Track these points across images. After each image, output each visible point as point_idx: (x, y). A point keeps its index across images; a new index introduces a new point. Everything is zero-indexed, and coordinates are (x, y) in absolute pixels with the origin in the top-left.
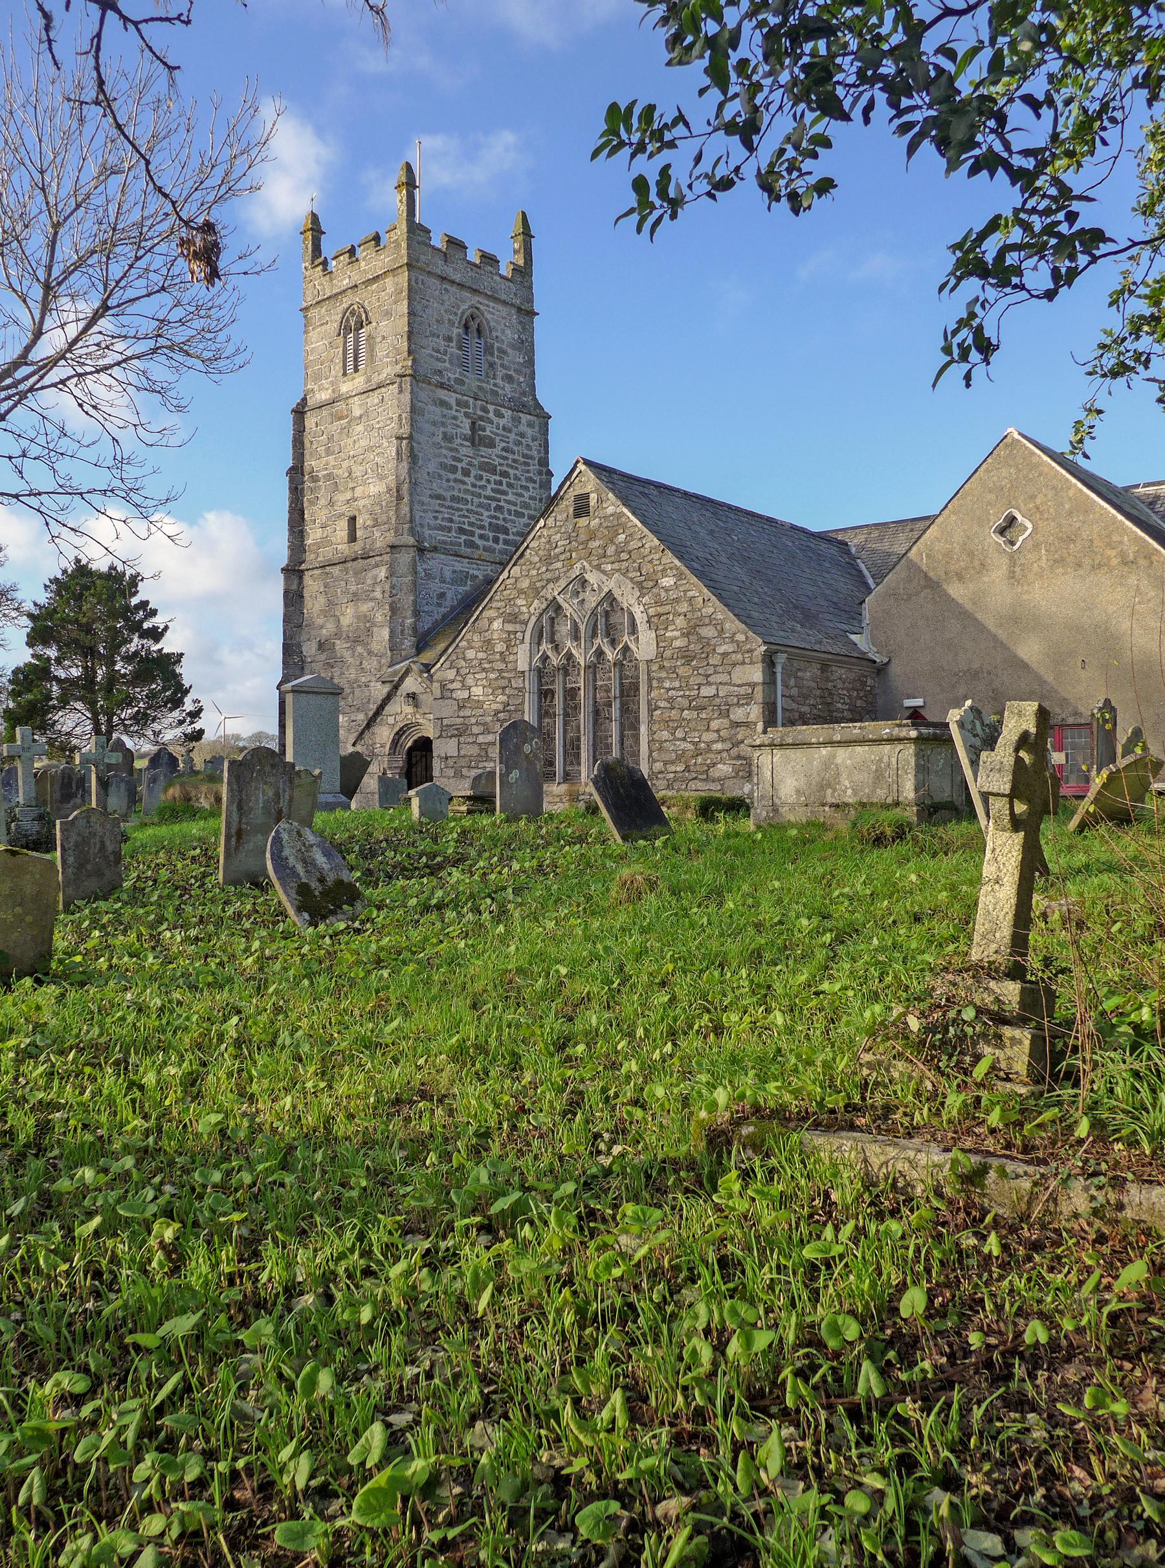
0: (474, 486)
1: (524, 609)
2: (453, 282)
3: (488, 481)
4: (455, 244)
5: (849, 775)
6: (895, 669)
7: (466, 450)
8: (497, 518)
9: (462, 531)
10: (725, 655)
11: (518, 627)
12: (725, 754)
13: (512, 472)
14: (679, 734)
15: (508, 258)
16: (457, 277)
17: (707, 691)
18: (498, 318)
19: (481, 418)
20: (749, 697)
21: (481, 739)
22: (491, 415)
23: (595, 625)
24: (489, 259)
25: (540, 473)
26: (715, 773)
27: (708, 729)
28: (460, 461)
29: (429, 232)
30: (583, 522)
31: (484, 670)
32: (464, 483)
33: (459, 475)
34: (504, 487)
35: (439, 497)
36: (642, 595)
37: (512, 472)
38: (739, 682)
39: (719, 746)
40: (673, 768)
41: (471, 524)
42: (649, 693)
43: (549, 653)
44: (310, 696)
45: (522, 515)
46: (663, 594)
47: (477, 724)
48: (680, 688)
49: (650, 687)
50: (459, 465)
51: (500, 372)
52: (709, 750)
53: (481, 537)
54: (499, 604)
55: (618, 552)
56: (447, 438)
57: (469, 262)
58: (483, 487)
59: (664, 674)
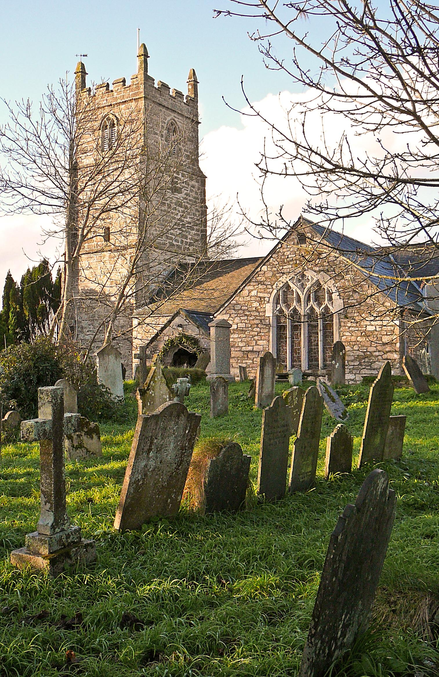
2: (164, 106)
3: (179, 211)
4: (165, 86)
11: (266, 295)
12: (380, 357)
15: (186, 91)
16: (165, 104)
22: (180, 176)
24: (179, 94)
26: (375, 366)
27: (371, 346)
31: (246, 315)
39: (377, 353)
40: (353, 364)
43: (284, 309)
48: (356, 327)
54: (255, 284)
57: (171, 96)
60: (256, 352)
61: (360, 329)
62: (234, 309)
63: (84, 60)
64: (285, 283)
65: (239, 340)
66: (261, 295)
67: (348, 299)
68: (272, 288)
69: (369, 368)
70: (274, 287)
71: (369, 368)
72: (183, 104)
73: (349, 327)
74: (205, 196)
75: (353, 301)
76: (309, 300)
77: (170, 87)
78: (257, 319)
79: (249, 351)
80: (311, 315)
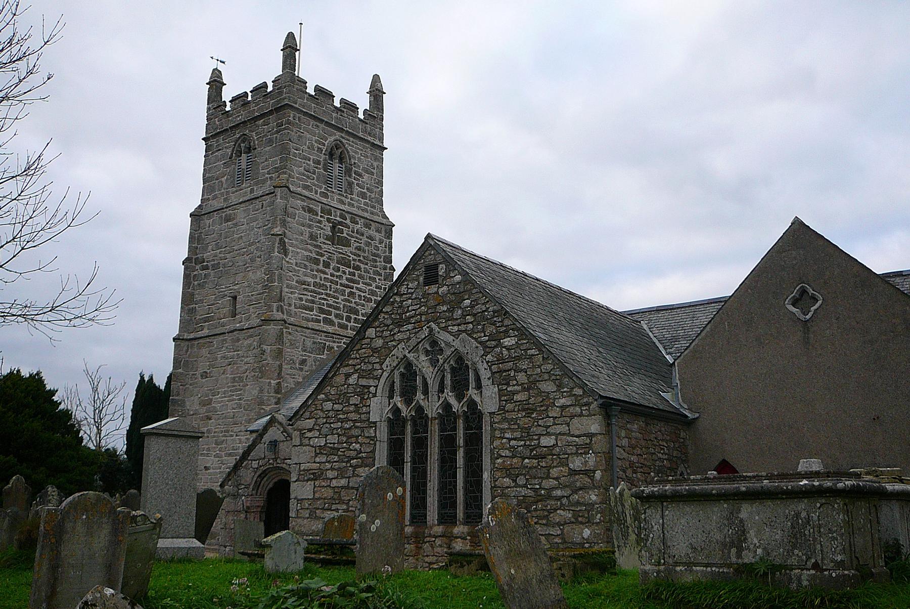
0: (332, 275)
1: (377, 366)
3: (344, 273)
5: (758, 532)
7: (328, 247)
8: (351, 302)
9: (322, 311)
10: (563, 407)
11: (372, 382)
13: (362, 266)
14: (521, 481)
17: (547, 441)
18: (353, 148)
19: (340, 223)
20: (588, 447)
21: (334, 483)
22: (348, 222)
24: (351, 107)
25: (385, 268)
28: (322, 255)
30: (433, 289)
31: (339, 420)
32: (325, 273)
33: (321, 267)
34: (356, 278)
35: (304, 283)
37: (362, 266)
38: (577, 433)
39: (559, 493)
41: (329, 306)
42: (492, 443)
44: (180, 443)
45: (370, 300)
46: (505, 352)
47: (332, 469)
50: (322, 259)
51: (357, 189)
52: (549, 497)
53: (337, 316)
55: (464, 316)
56: (313, 237)
57: (336, 107)
58: (340, 277)
59: (506, 426)
60: (353, 488)
61: (528, 443)
62: (322, 410)
63: (221, 67)
64: (402, 359)
65: (328, 466)
66: (363, 382)
67: (508, 384)
68: (382, 369)
69: (544, 522)
70: (384, 366)
71: (544, 522)
72: (357, 120)
73: (510, 440)
74: (391, 253)
75: (516, 387)
76: (441, 390)
77: (334, 94)
78: (357, 427)
79: (342, 487)
80: (447, 415)
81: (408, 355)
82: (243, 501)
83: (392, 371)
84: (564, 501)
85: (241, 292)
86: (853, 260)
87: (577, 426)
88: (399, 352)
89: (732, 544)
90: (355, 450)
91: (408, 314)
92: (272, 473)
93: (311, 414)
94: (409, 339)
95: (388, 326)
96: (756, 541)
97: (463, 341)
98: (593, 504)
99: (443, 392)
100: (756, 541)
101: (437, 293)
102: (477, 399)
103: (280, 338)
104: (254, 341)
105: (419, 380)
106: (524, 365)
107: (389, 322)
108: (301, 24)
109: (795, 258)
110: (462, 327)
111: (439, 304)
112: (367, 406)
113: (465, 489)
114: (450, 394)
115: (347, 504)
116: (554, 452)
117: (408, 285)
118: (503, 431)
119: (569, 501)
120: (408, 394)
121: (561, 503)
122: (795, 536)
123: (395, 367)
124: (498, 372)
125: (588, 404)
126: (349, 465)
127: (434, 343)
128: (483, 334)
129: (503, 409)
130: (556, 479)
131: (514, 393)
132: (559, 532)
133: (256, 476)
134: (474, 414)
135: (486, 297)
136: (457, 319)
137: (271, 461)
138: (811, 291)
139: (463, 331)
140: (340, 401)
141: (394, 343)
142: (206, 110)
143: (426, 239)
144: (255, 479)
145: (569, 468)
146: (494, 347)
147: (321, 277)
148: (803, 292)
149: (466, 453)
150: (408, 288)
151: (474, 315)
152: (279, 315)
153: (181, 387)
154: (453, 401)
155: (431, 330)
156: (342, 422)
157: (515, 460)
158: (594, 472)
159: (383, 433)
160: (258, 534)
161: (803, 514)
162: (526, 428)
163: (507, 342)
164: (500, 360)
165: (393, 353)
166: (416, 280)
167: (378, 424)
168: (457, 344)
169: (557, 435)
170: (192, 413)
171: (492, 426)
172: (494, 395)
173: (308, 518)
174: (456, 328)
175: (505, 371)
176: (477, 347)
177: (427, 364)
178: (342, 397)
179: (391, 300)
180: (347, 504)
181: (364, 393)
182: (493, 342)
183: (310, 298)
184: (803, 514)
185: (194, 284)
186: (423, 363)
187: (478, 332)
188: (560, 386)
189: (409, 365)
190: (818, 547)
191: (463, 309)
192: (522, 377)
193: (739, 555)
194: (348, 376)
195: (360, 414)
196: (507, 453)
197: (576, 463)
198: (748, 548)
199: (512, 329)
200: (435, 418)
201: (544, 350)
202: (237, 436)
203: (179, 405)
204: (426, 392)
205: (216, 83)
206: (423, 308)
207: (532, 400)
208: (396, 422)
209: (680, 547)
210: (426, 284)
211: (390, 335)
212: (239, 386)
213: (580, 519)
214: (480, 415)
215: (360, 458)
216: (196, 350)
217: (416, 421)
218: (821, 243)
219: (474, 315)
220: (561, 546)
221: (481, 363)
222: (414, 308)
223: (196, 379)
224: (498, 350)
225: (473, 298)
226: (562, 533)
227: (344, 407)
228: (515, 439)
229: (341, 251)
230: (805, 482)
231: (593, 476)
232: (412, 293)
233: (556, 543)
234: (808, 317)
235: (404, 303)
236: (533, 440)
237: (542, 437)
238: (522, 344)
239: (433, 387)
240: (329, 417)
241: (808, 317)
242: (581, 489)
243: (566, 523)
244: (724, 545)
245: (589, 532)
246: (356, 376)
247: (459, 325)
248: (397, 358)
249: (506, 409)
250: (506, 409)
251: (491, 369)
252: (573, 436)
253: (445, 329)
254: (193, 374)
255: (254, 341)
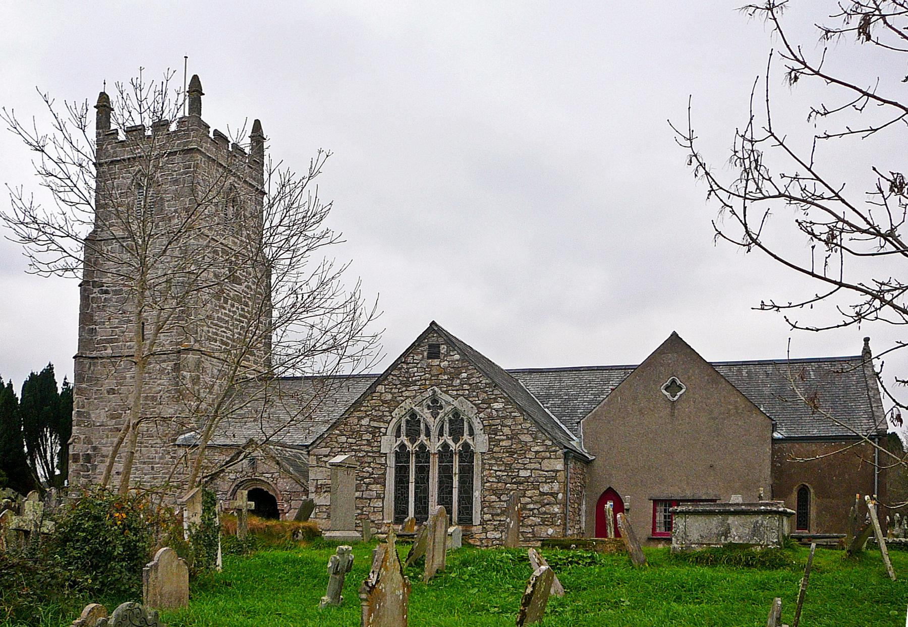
3: (238, 309)
6: (598, 463)
9: (222, 342)
10: (537, 452)
11: (382, 425)
17: (523, 473)
23: (442, 427)
29: (209, 127)
30: (436, 362)
32: (224, 308)
36: (479, 412)
39: (532, 506)
42: (482, 472)
46: (494, 412)
49: (483, 469)
58: (234, 312)
59: (493, 462)
60: (366, 499)
61: (510, 474)
68: (392, 416)
73: (496, 471)
76: (441, 434)
80: (445, 453)
81: (414, 408)
82: (221, 504)
83: (400, 418)
84: (536, 511)
85: (149, 320)
86: (695, 357)
87: (546, 464)
88: (407, 404)
89: (722, 534)
90: (368, 472)
91: (414, 378)
92: (248, 483)
93: (326, 444)
94: (415, 397)
95: (396, 385)
96: (735, 533)
97: (461, 402)
98: (556, 514)
99: (442, 435)
100: (735, 533)
101: (439, 365)
102: (471, 442)
103: (198, 364)
104: (168, 366)
105: (422, 426)
106: (509, 422)
107: (397, 382)
108: (186, 57)
109: (671, 359)
110: (460, 392)
111: (441, 374)
112: (378, 442)
113: (459, 502)
114: (449, 438)
115: (362, 510)
116: (529, 480)
117: (413, 357)
118: (491, 465)
119: (539, 511)
120: (413, 434)
121: (533, 513)
122: (755, 531)
123: (403, 416)
124: (488, 425)
125: (555, 451)
126: (362, 482)
127: (435, 401)
128: (477, 399)
129: (492, 451)
130: (530, 497)
131: (500, 441)
132: (531, 531)
133: (234, 485)
134: (467, 454)
135: (480, 373)
136: (456, 386)
137: (249, 474)
138: (679, 382)
139: (461, 395)
140: (354, 437)
141: (402, 398)
142: (95, 135)
143: (431, 324)
144: (233, 487)
145: (540, 491)
146: (486, 408)
147: (222, 313)
148: (674, 381)
149: (460, 478)
150: (414, 359)
151: (470, 385)
152: (197, 346)
153: (85, 401)
154: (450, 442)
155: (435, 392)
156: (356, 452)
157: (500, 484)
158: (557, 494)
159: (391, 462)
160: (303, 528)
161: (760, 522)
162: (508, 464)
163: (496, 406)
164: (490, 417)
165: (401, 405)
166: (421, 354)
167: (388, 455)
168: (456, 403)
169: (531, 470)
170: (98, 424)
171: (482, 461)
172: (485, 441)
173: (325, 519)
174: (455, 393)
175: (494, 425)
176: (472, 407)
177: (430, 415)
178: (355, 433)
179: (399, 366)
180: (362, 510)
181: (375, 432)
182: (485, 405)
183: (214, 331)
184: (760, 522)
185: (92, 306)
186: (427, 415)
187: (473, 397)
188: (535, 438)
189: (413, 415)
190: (766, 536)
191: (461, 380)
192: (506, 430)
193: (725, 539)
194: (360, 419)
195: (372, 447)
196: (494, 480)
197: (545, 488)
198: (731, 536)
199: (500, 398)
200: (436, 454)
201: (524, 413)
202: (152, 447)
203: (85, 417)
204: (428, 435)
205: (104, 106)
206: (427, 375)
207: (514, 446)
208: (402, 454)
209: (694, 536)
210: (429, 358)
211: (399, 392)
212: (153, 404)
213: (546, 523)
214: (472, 454)
215: (372, 478)
216: (99, 368)
217: (419, 455)
218: (689, 351)
219: (470, 385)
220: (532, 539)
221: (475, 419)
222: (420, 374)
223: (101, 394)
224: (489, 410)
225: (469, 372)
226: (533, 531)
227: (357, 441)
228: (500, 471)
229: (235, 289)
230: (762, 508)
231: (557, 497)
232: (418, 363)
233: (529, 537)
234: (675, 399)
235: (410, 370)
236: (514, 472)
237: (521, 471)
238: (508, 408)
239: (434, 431)
240: (343, 447)
241: (675, 399)
242: (548, 504)
243: (536, 525)
244: (718, 535)
245: (552, 531)
246: (367, 419)
247: (457, 390)
248: (405, 409)
249: (494, 451)
250: (494, 451)
251: (482, 423)
252: (543, 471)
253: (446, 392)
254: (97, 390)
255: (168, 366)
